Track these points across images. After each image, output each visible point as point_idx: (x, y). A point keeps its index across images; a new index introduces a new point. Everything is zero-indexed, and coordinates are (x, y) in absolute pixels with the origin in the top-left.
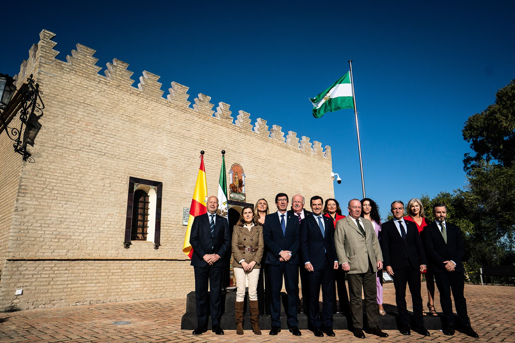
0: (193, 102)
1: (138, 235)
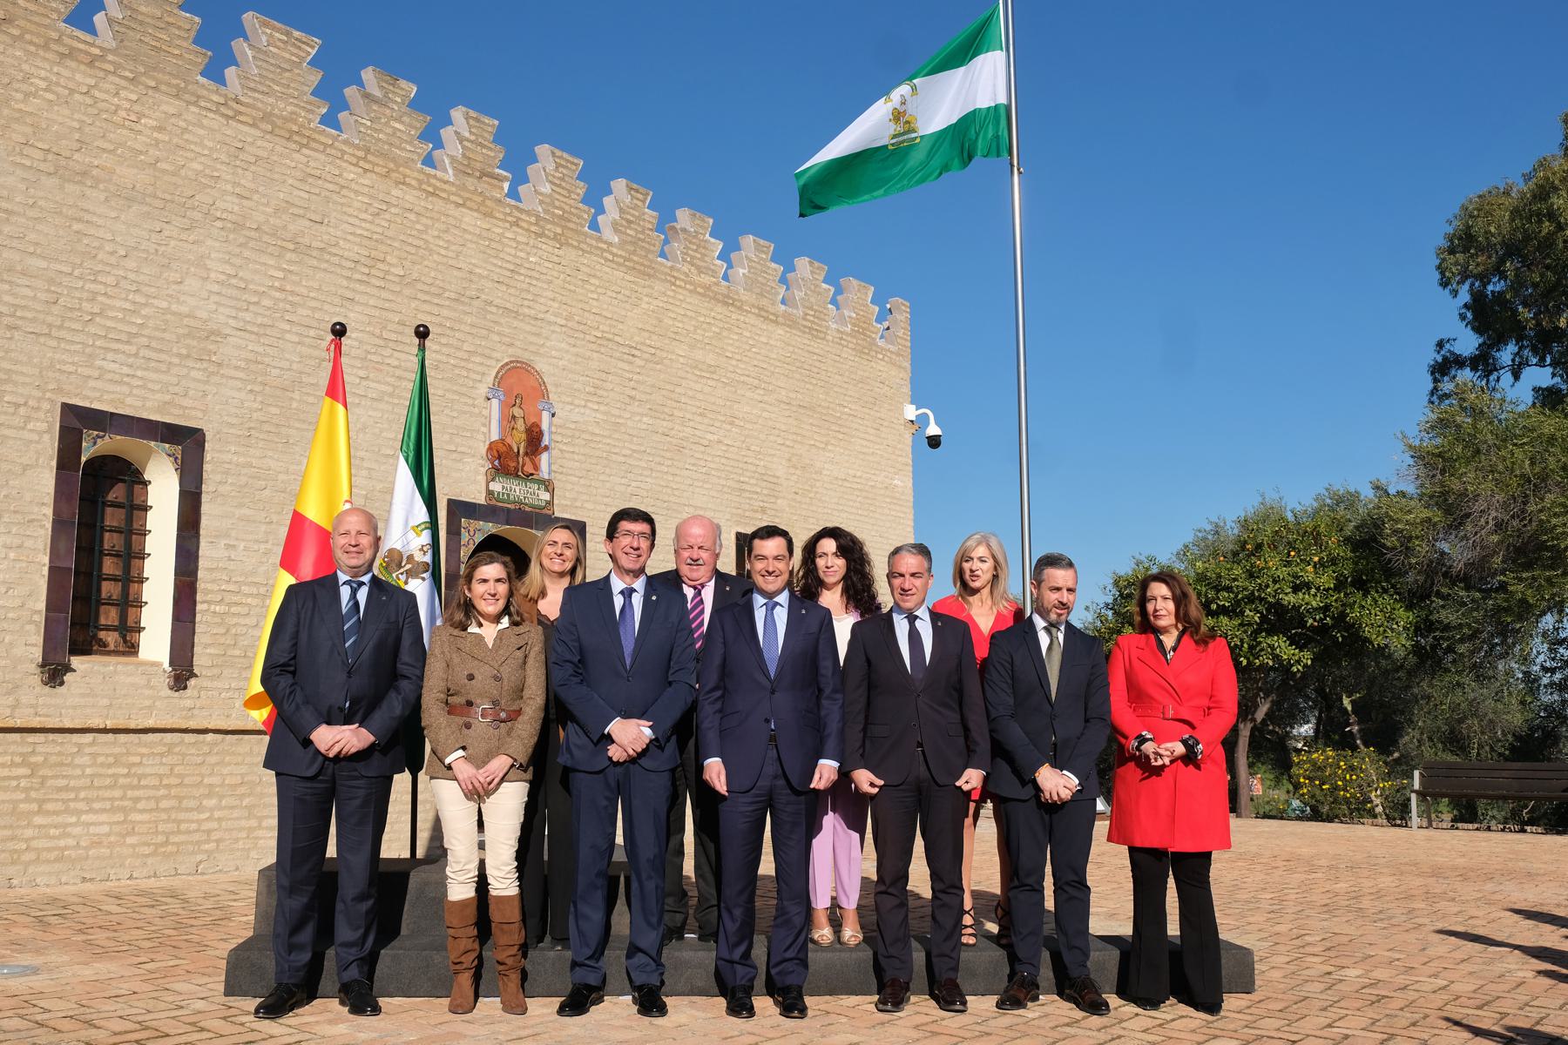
1: (102, 635)
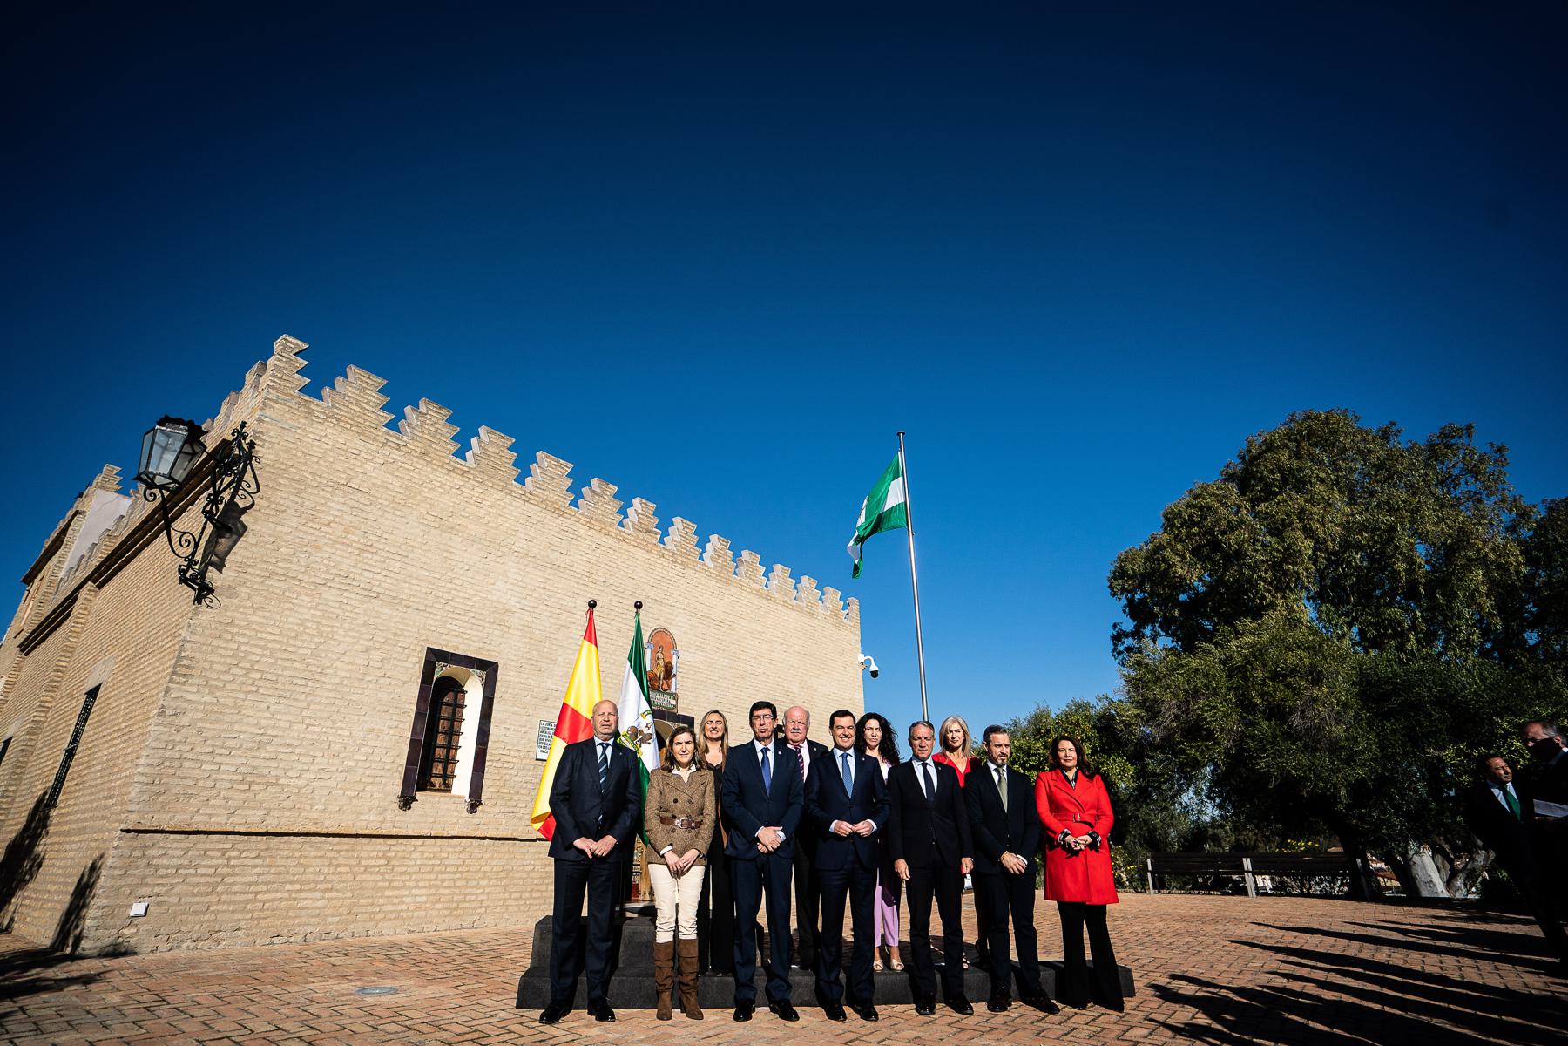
0: (580, 496)
